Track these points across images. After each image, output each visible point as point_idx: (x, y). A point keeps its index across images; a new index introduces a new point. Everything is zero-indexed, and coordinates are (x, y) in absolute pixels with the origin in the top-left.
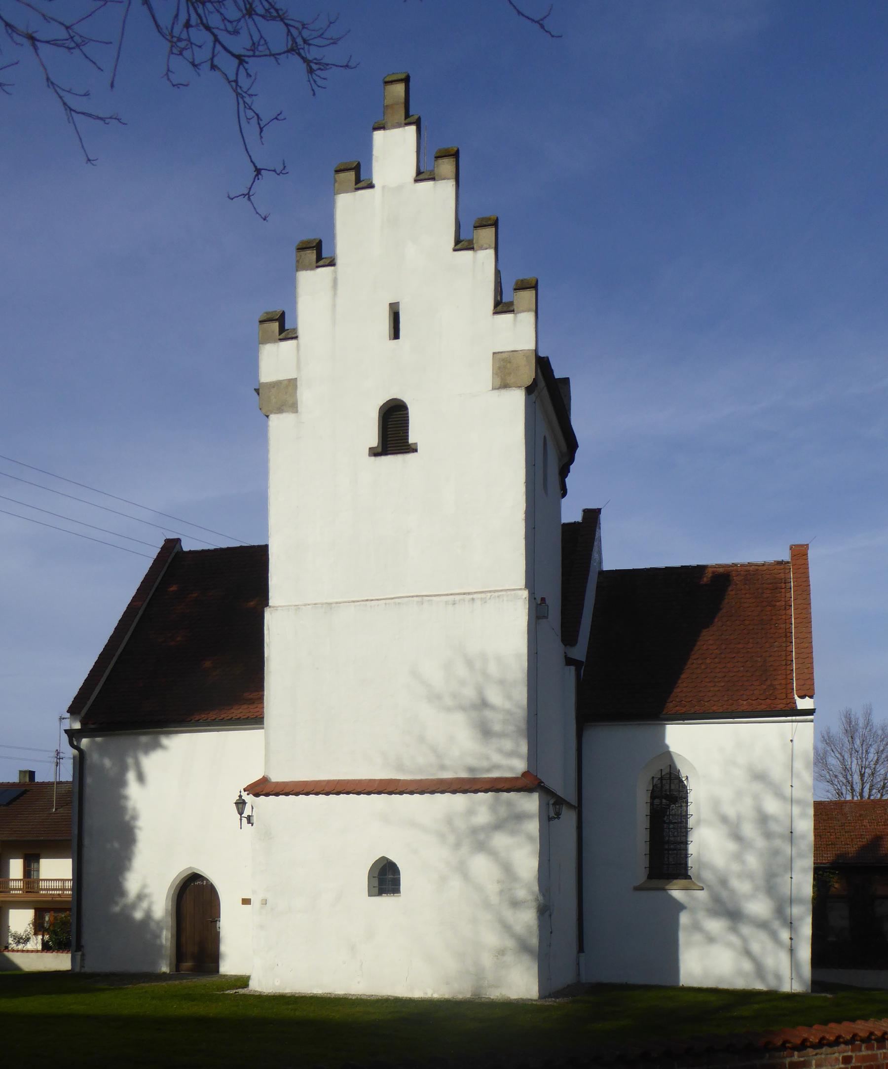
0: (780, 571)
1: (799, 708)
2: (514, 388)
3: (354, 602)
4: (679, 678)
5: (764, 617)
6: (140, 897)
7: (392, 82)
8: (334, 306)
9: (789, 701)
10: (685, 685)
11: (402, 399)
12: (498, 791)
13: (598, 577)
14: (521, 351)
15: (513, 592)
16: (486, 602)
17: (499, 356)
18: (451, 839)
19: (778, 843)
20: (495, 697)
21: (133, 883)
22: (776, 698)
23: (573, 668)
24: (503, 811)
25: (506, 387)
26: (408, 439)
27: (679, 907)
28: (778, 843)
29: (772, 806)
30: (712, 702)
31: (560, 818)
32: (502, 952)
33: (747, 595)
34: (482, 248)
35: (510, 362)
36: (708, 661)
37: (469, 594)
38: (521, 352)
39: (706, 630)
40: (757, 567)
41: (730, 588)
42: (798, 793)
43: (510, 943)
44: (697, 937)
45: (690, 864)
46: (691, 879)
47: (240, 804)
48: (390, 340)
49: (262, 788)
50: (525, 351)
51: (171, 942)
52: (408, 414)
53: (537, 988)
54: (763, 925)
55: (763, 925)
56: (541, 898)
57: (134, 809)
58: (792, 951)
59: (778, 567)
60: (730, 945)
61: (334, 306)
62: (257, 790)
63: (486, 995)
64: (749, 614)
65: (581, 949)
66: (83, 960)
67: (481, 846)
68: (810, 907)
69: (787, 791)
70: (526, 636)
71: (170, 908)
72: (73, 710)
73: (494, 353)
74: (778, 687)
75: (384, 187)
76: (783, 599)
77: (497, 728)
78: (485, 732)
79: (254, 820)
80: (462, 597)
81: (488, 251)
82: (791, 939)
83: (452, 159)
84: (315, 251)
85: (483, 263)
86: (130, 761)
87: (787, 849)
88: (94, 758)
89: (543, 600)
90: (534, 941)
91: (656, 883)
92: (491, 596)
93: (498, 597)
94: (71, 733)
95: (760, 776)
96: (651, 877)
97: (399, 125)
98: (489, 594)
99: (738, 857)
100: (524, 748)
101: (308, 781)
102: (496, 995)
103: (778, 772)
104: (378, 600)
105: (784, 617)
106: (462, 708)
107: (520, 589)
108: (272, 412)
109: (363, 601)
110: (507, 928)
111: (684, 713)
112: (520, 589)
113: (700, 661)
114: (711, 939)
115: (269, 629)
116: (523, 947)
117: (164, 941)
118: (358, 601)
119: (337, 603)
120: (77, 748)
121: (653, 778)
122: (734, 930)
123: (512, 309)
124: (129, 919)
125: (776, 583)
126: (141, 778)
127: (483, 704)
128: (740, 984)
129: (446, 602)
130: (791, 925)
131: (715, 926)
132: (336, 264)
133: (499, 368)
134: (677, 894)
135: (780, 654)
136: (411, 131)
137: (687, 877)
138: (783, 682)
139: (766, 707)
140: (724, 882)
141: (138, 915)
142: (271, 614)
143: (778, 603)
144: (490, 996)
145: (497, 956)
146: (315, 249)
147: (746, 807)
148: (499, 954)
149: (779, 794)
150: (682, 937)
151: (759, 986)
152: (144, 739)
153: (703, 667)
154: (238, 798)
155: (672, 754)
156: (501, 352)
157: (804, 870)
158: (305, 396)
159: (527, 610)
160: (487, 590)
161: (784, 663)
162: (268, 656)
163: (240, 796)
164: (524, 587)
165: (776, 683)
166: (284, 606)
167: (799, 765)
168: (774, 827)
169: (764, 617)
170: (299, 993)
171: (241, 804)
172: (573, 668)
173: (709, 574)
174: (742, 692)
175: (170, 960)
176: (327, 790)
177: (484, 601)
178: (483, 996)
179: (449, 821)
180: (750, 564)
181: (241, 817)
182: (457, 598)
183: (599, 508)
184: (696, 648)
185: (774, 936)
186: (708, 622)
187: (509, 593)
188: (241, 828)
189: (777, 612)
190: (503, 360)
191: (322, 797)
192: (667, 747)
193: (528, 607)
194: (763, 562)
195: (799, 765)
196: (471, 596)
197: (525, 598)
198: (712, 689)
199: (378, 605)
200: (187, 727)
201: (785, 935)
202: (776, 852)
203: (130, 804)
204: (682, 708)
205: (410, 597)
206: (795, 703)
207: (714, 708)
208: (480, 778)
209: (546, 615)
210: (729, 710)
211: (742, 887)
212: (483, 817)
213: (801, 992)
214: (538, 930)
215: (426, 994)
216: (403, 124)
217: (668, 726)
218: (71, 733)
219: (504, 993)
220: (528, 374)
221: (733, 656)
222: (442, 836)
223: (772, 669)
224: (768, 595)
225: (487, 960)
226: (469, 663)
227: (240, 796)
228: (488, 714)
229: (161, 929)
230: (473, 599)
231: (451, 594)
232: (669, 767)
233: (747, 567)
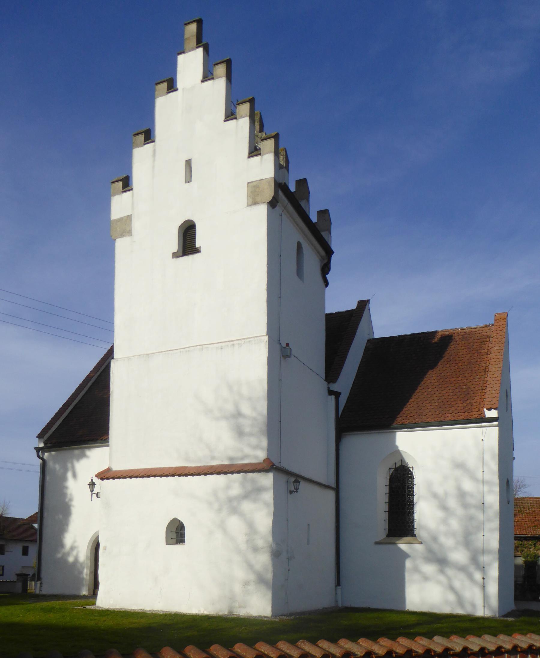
0: (487, 331)
1: (487, 416)
2: (261, 204)
3: (162, 352)
4: (408, 402)
5: (472, 360)
6: (72, 548)
7: (189, 23)
8: (153, 167)
9: (480, 412)
10: (411, 406)
11: (192, 220)
12: (246, 472)
13: (367, 343)
14: (265, 179)
15: (258, 338)
16: (241, 346)
17: (251, 184)
18: (216, 506)
19: (473, 511)
20: (246, 409)
21: (69, 540)
22: (472, 411)
23: (333, 397)
24: (249, 487)
25: (256, 204)
26: (195, 244)
27: (405, 556)
28: (473, 511)
29: (468, 486)
30: (419, 413)
31: (298, 491)
32: (246, 583)
33: (463, 348)
34: (242, 117)
35: (258, 188)
36: (430, 390)
37: (231, 341)
38: (265, 180)
39: (431, 371)
40: (471, 330)
41: (452, 343)
42: (487, 477)
43: (252, 577)
44: (416, 577)
45: (415, 527)
46: (416, 537)
47: (92, 484)
48: (186, 183)
49: (104, 475)
50: (268, 179)
51: (90, 577)
52: (196, 230)
53: (271, 609)
54: (462, 569)
55: (462, 569)
56: (274, 546)
57: (71, 495)
58: (484, 587)
59: (486, 328)
60: (439, 582)
61: (153, 167)
62: (102, 476)
63: (237, 613)
64: (463, 359)
65: (338, 583)
66: (41, 586)
67: (234, 511)
68: (497, 556)
69: (480, 475)
70: (266, 367)
71: (89, 555)
72: (40, 436)
73: (248, 183)
74: (474, 404)
75: (183, 89)
76: (486, 348)
77: (247, 430)
78: (240, 433)
79: (101, 495)
80: (227, 343)
81: (245, 118)
82: (483, 578)
83: (224, 64)
84: (143, 135)
85: (242, 127)
86: (69, 465)
87: (480, 516)
88: (50, 464)
89: (288, 345)
90: (269, 576)
91: (392, 539)
92: (245, 341)
93: (249, 342)
94: (38, 450)
95: (460, 466)
96: (388, 535)
97: (193, 49)
98: (243, 341)
99: (445, 521)
100: (264, 443)
101: (133, 469)
102: (243, 613)
103: (472, 462)
104: (176, 350)
105: (485, 359)
106: (226, 418)
107: (263, 336)
108: (117, 238)
109: (168, 351)
110: (250, 566)
111: (408, 424)
112: (263, 336)
113: (424, 391)
114: (426, 578)
115: (113, 373)
116: (261, 580)
117: (85, 576)
118: (164, 352)
119: (152, 354)
120: (42, 459)
121: (390, 469)
122: (442, 571)
123: (259, 153)
124: (66, 562)
125: (483, 339)
126: (75, 475)
127: (239, 414)
128: (446, 610)
129: (217, 347)
130: (483, 569)
131: (429, 569)
132: (155, 141)
133: (252, 192)
134: (403, 547)
135: (479, 383)
136: (200, 52)
137: (414, 535)
138: (478, 401)
139: (464, 417)
140: (435, 539)
141: (71, 559)
142: (114, 363)
143: (482, 351)
144: (239, 614)
145: (245, 586)
146: (143, 133)
147: (450, 487)
148: (246, 584)
149: (474, 478)
150: (407, 575)
151: (460, 611)
152: (77, 452)
153: (426, 394)
154: (91, 481)
155: (401, 451)
156: (253, 182)
157: (492, 530)
158: (136, 225)
159: (267, 349)
160: (243, 338)
161: (480, 388)
162: (112, 391)
163: (92, 480)
164: (266, 334)
165: (473, 401)
166: (122, 358)
167: (487, 457)
168: (470, 500)
169: (472, 360)
170: (124, 609)
171: (92, 485)
172: (333, 397)
173: (439, 336)
174: (449, 408)
175: (89, 587)
176: (142, 474)
177: (240, 345)
178: (235, 614)
179: (215, 493)
180: (467, 328)
181: (92, 493)
182: (224, 344)
183: (368, 299)
184: (423, 383)
185: (470, 577)
186: (432, 366)
187: (256, 338)
188: (92, 501)
189: (481, 357)
190: (254, 187)
191: (139, 479)
192: (397, 447)
193: (268, 347)
194: (476, 326)
195: (487, 457)
196: (232, 343)
197: (266, 341)
198: (429, 407)
199: (176, 353)
200: (101, 443)
201: (478, 576)
202: (471, 518)
203: (69, 492)
204: (406, 421)
205: (195, 346)
206: (485, 414)
207: (429, 420)
208: (237, 464)
209: (289, 354)
210: (438, 421)
211: (448, 542)
212: (236, 490)
213: (491, 616)
214: (272, 568)
215: (200, 611)
216: (195, 48)
217: (397, 433)
218: (38, 450)
219: (248, 612)
220: (269, 193)
221: (447, 386)
222: (210, 504)
223: (472, 393)
224: (477, 346)
225: (238, 588)
226: (230, 388)
227: (92, 480)
228: (241, 421)
229: (83, 568)
230: (233, 345)
231: (220, 343)
232: (401, 461)
233: (465, 330)
